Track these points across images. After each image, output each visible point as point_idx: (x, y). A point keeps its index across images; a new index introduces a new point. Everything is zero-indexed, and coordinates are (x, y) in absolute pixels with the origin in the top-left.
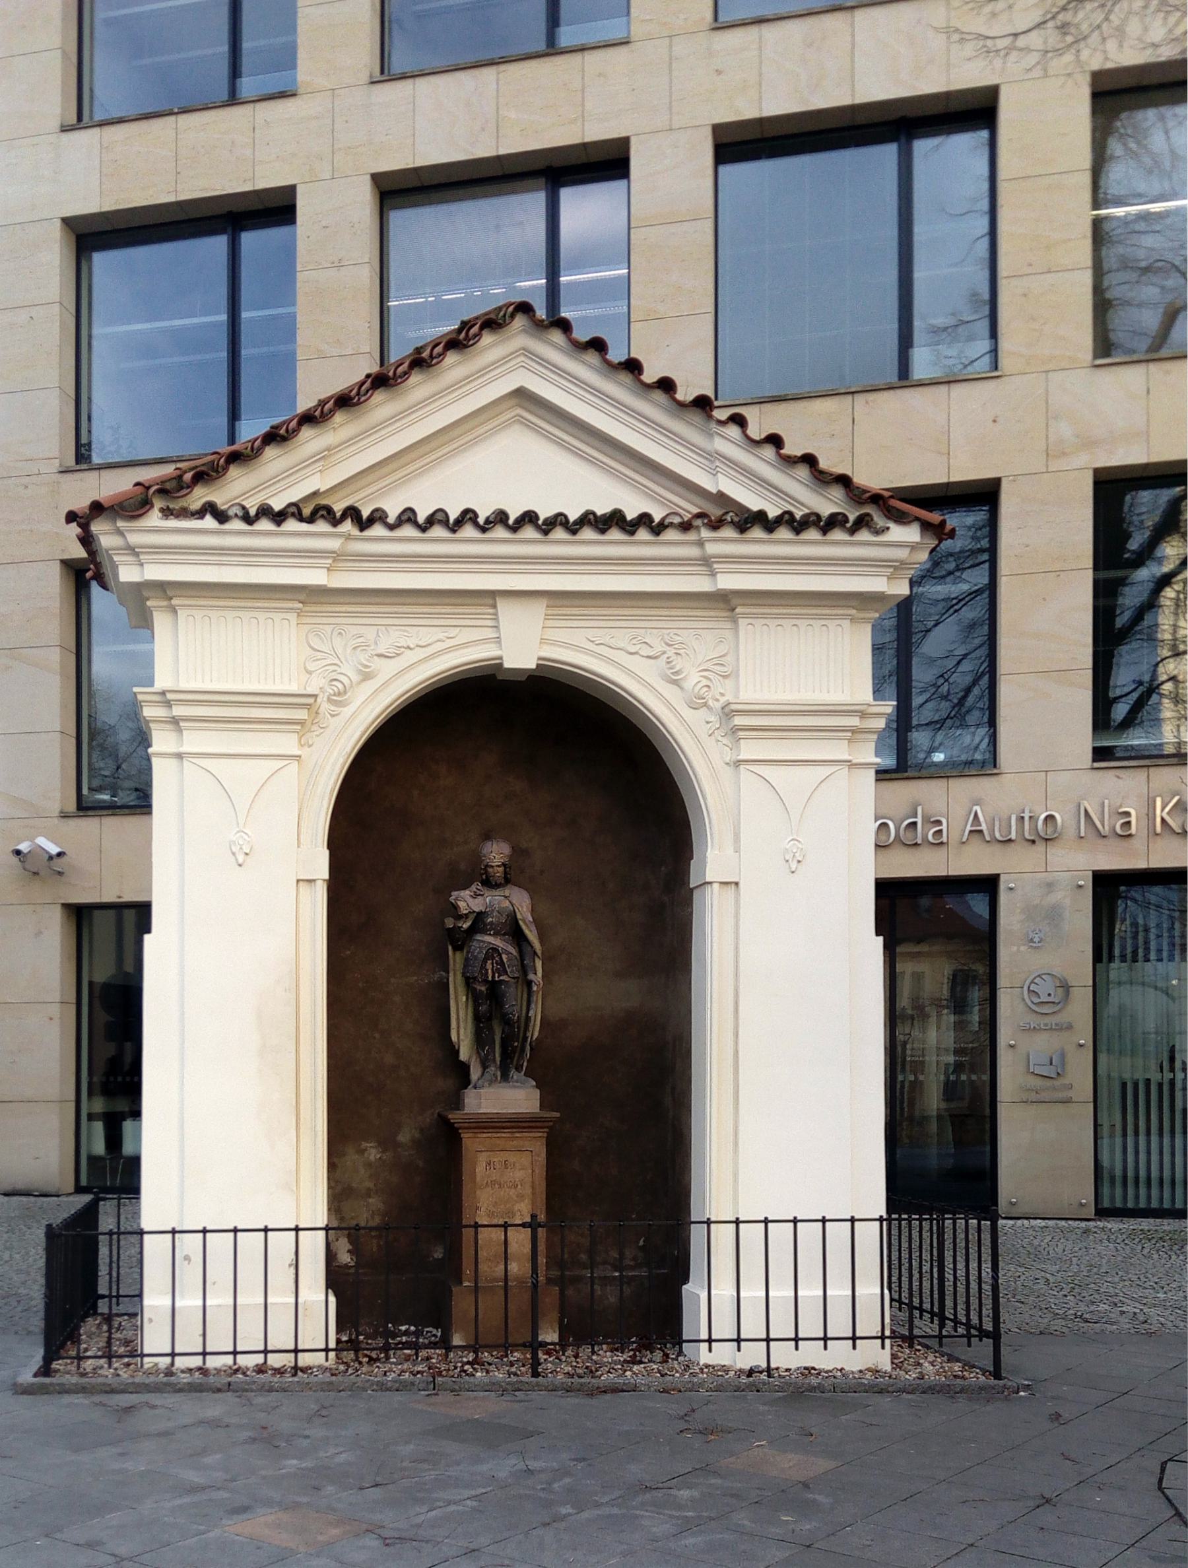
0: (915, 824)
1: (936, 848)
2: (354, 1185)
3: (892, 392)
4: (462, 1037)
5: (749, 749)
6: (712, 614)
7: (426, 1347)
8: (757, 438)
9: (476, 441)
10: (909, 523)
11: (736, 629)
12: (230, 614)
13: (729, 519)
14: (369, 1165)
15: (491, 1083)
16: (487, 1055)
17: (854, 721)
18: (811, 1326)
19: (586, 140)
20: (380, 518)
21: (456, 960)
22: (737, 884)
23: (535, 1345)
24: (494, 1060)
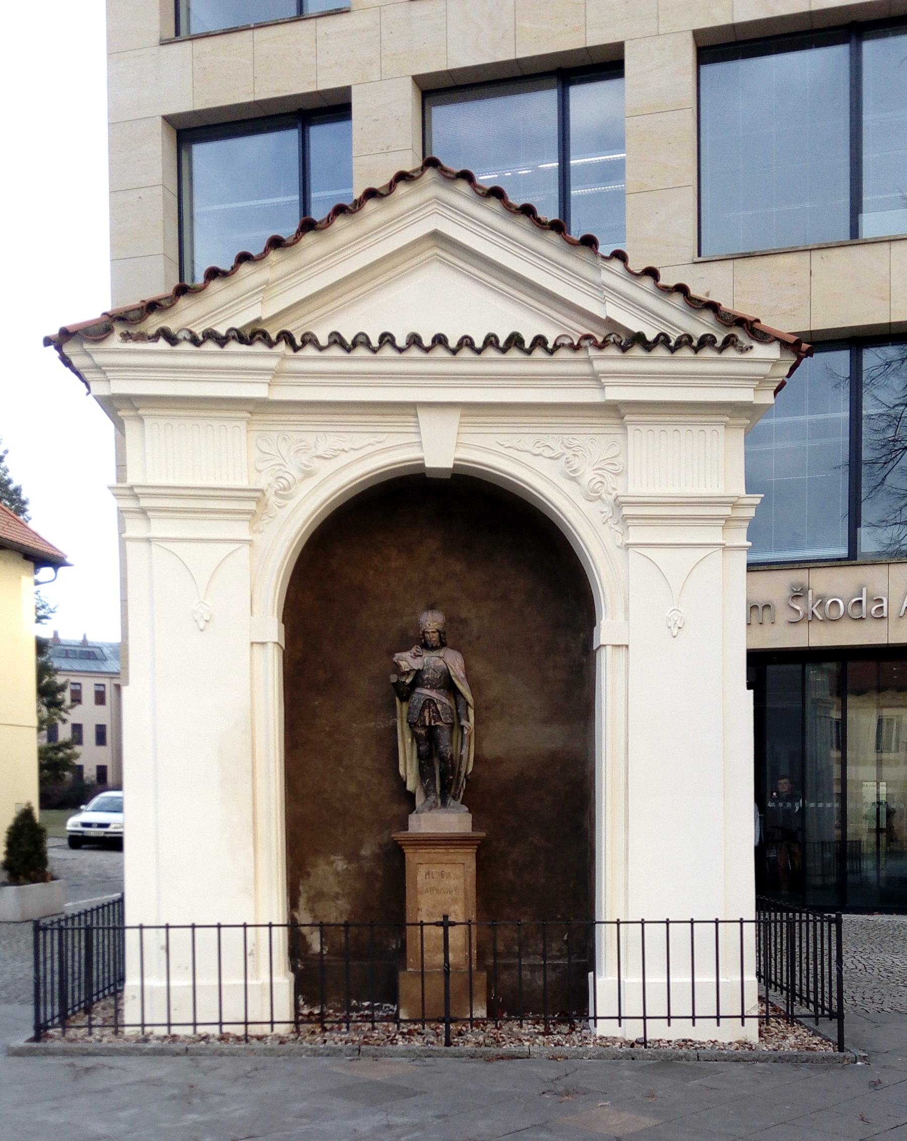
0: (860, 602)
1: (875, 620)
2: (325, 890)
3: (843, 249)
4: (408, 771)
5: (637, 535)
6: (601, 421)
7: (383, 1019)
8: (638, 272)
9: (403, 275)
10: (771, 342)
11: (626, 434)
12: (216, 424)
13: (612, 340)
14: (337, 874)
15: (430, 809)
16: (428, 786)
17: (727, 511)
18: (681, 1007)
19: (588, 45)
20: (310, 341)
21: (402, 709)
22: (627, 646)
23: (448, 1020)
24: (435, 791)
